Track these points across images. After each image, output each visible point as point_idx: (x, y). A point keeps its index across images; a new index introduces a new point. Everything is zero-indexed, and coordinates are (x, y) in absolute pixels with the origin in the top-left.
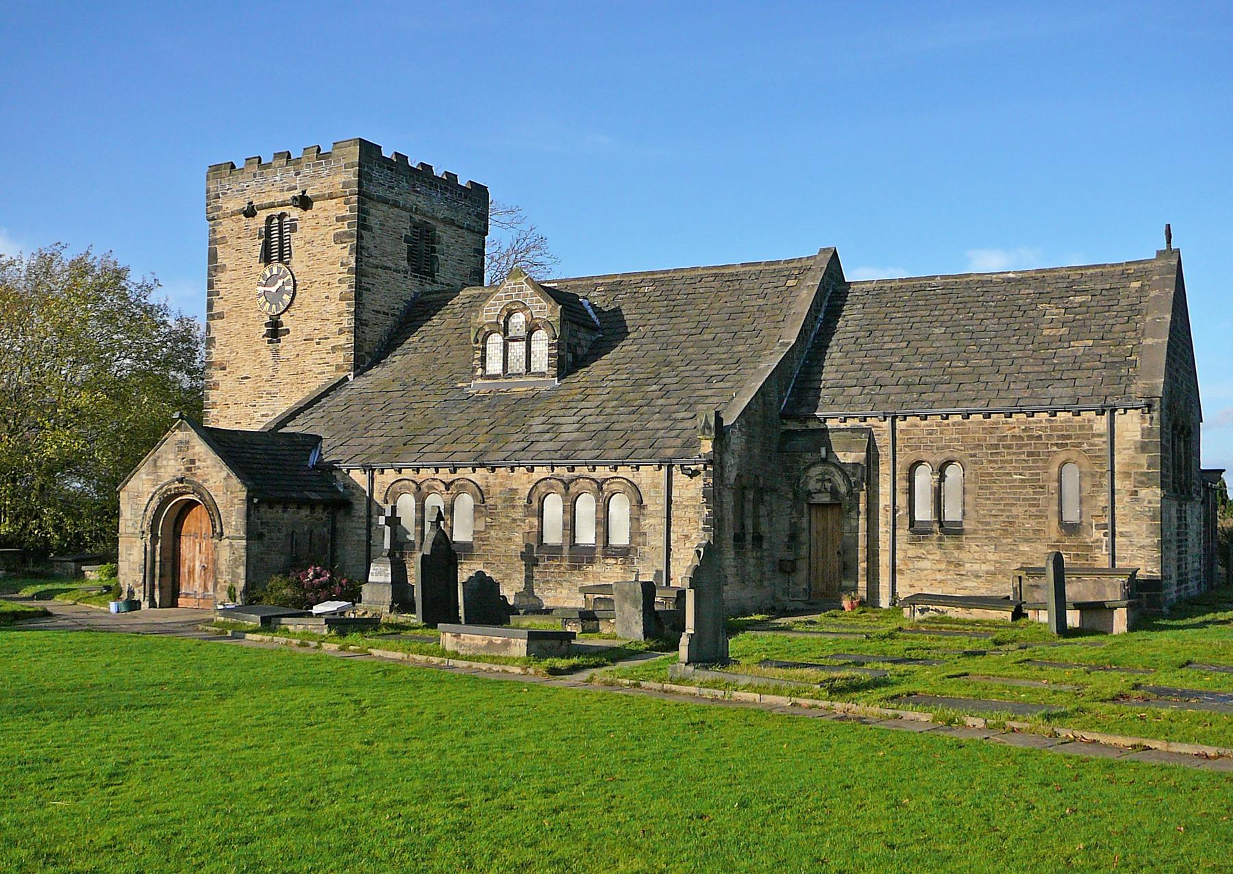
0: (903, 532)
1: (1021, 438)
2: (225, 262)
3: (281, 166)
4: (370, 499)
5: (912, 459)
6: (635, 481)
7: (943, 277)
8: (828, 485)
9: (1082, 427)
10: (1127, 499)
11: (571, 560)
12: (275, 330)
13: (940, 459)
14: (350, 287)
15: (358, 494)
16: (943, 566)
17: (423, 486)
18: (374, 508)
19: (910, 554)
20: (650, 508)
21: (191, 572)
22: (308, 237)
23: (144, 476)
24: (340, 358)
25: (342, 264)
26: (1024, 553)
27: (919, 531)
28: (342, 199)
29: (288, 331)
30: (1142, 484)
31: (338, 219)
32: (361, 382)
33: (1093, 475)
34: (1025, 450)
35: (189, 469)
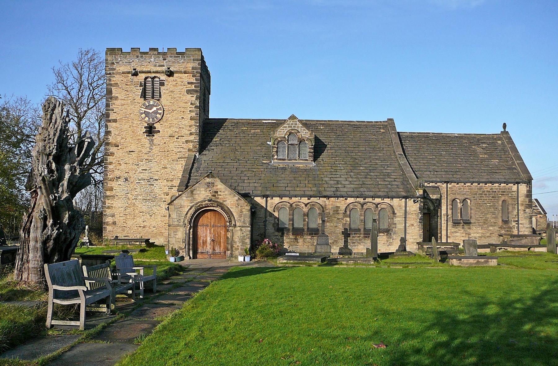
0: (450, 223)
1: (490, 192)
2: (117, 95)
3: (155, 55)
4: (266, 209)
5: (454, 198)
6: (391, 204)
7: (433, 133)
8: (426, 206)
9: (509, 189)
10: (522, 212)
11: (364, 234)
12: (150, 130)
13: (463, 198)
14: (196, 114)
15: (258, 207)
16: (464, 235)
17: (293, 205)
18: (268, 214)
19: (452, 231)
20: (398, 214)
21: (205, 243)
22: (171, 89)
23: (184, 198)
24: (191, 146)
25: (191, 104)
26: (490, 230)
27: (456, 223)
28: (191, 75)
29: (159, 132)
30: (527, 208)
31: (188, 83)
32: (204, 158)
33: (512, 205)
34: (491, 196)
35: (214, 196)
